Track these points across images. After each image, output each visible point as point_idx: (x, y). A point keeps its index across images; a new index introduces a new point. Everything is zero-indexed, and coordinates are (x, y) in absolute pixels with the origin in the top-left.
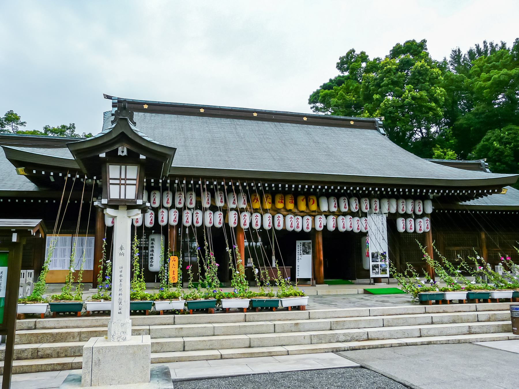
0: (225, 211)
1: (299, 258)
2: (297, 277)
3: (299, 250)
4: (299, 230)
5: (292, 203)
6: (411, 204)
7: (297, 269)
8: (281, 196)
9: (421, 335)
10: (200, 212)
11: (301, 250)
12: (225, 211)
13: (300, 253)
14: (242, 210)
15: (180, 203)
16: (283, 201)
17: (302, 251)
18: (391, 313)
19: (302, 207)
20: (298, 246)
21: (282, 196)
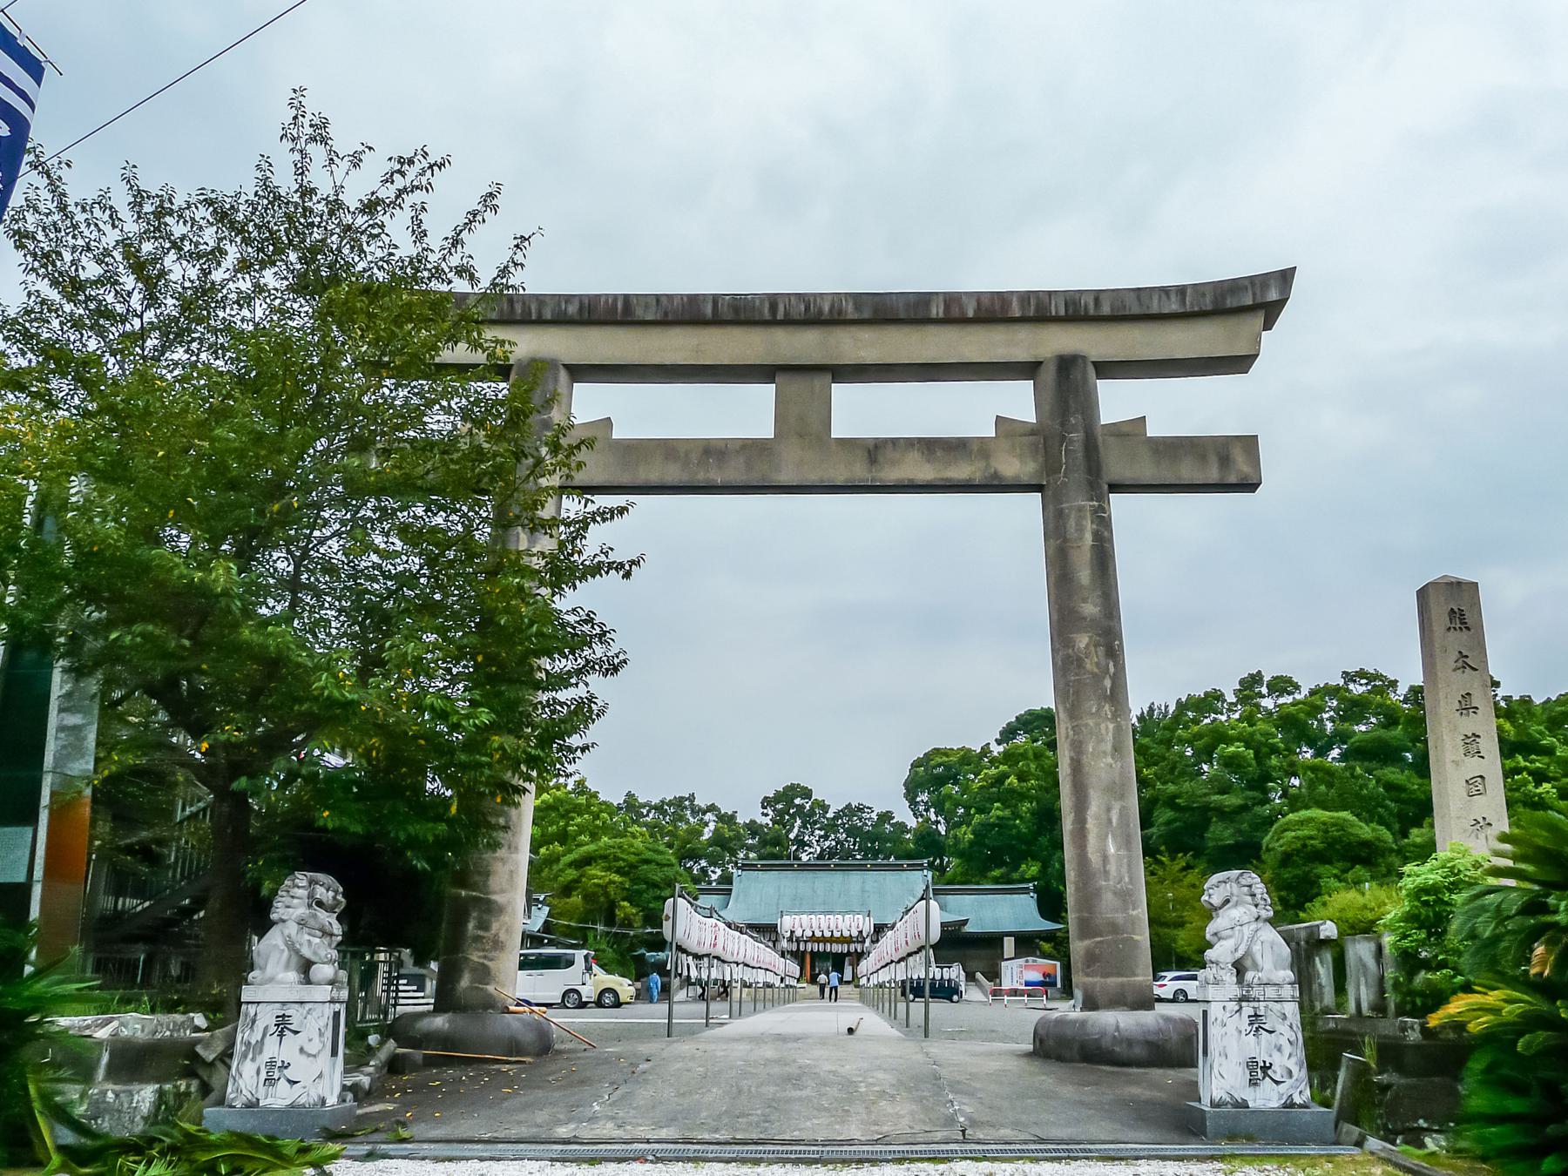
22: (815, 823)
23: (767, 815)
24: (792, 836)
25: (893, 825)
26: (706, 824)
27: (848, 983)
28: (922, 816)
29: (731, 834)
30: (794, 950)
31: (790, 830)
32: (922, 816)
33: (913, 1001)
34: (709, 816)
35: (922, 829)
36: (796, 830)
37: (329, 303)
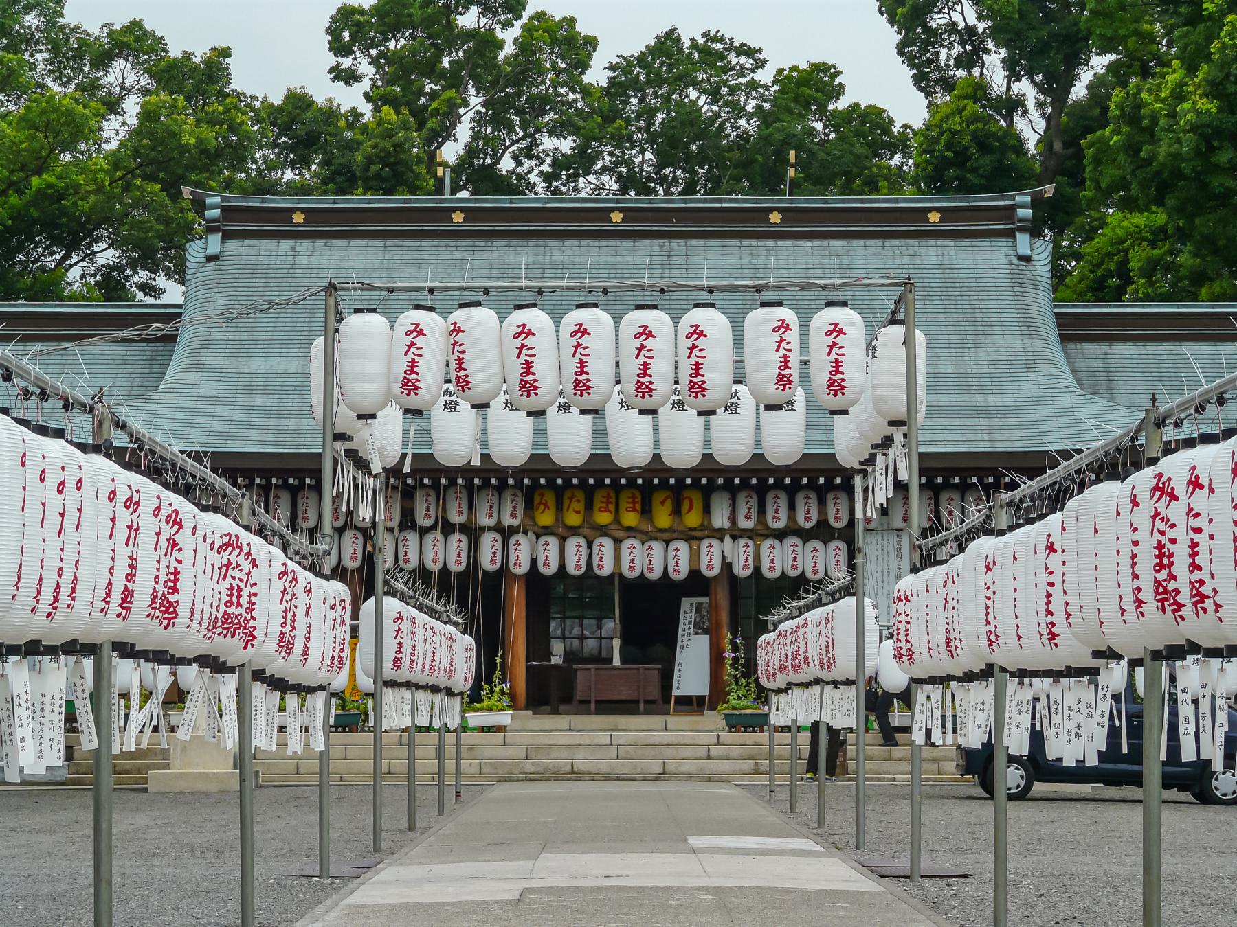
0: (471, 532)
1: (685, 644)
2: (675, 692)
3: (687, 622)
4: (656, 574)
5: (634, 510)
6: (928, 502)
7: (676, 673)
8: (605, 494)
9: (411, 745)
10: (412, 538)
11: (690, 623)
12: (471, 532)
13: (687, 631)
14: (513, 531)
15: (837, 519)
16: (612, 507)
17: (692, 626)
18: (651, 742)
19: (663, 518)
20: (685, 612)
21: (608, 494)
22: (540, 105)
23: (350, 77)
24: (450, 152)
25: (838, 121)
26: (113, 105)
27: (691, 704)
28: (948, 85)
29: (208, 133)
30: (455, 568)
31: (445, 132)
32: (948, 85)
33: (1022, 795)
34: (120, 74)
35: (956, 123)
36: (464, 131)
37: (80, 47)
